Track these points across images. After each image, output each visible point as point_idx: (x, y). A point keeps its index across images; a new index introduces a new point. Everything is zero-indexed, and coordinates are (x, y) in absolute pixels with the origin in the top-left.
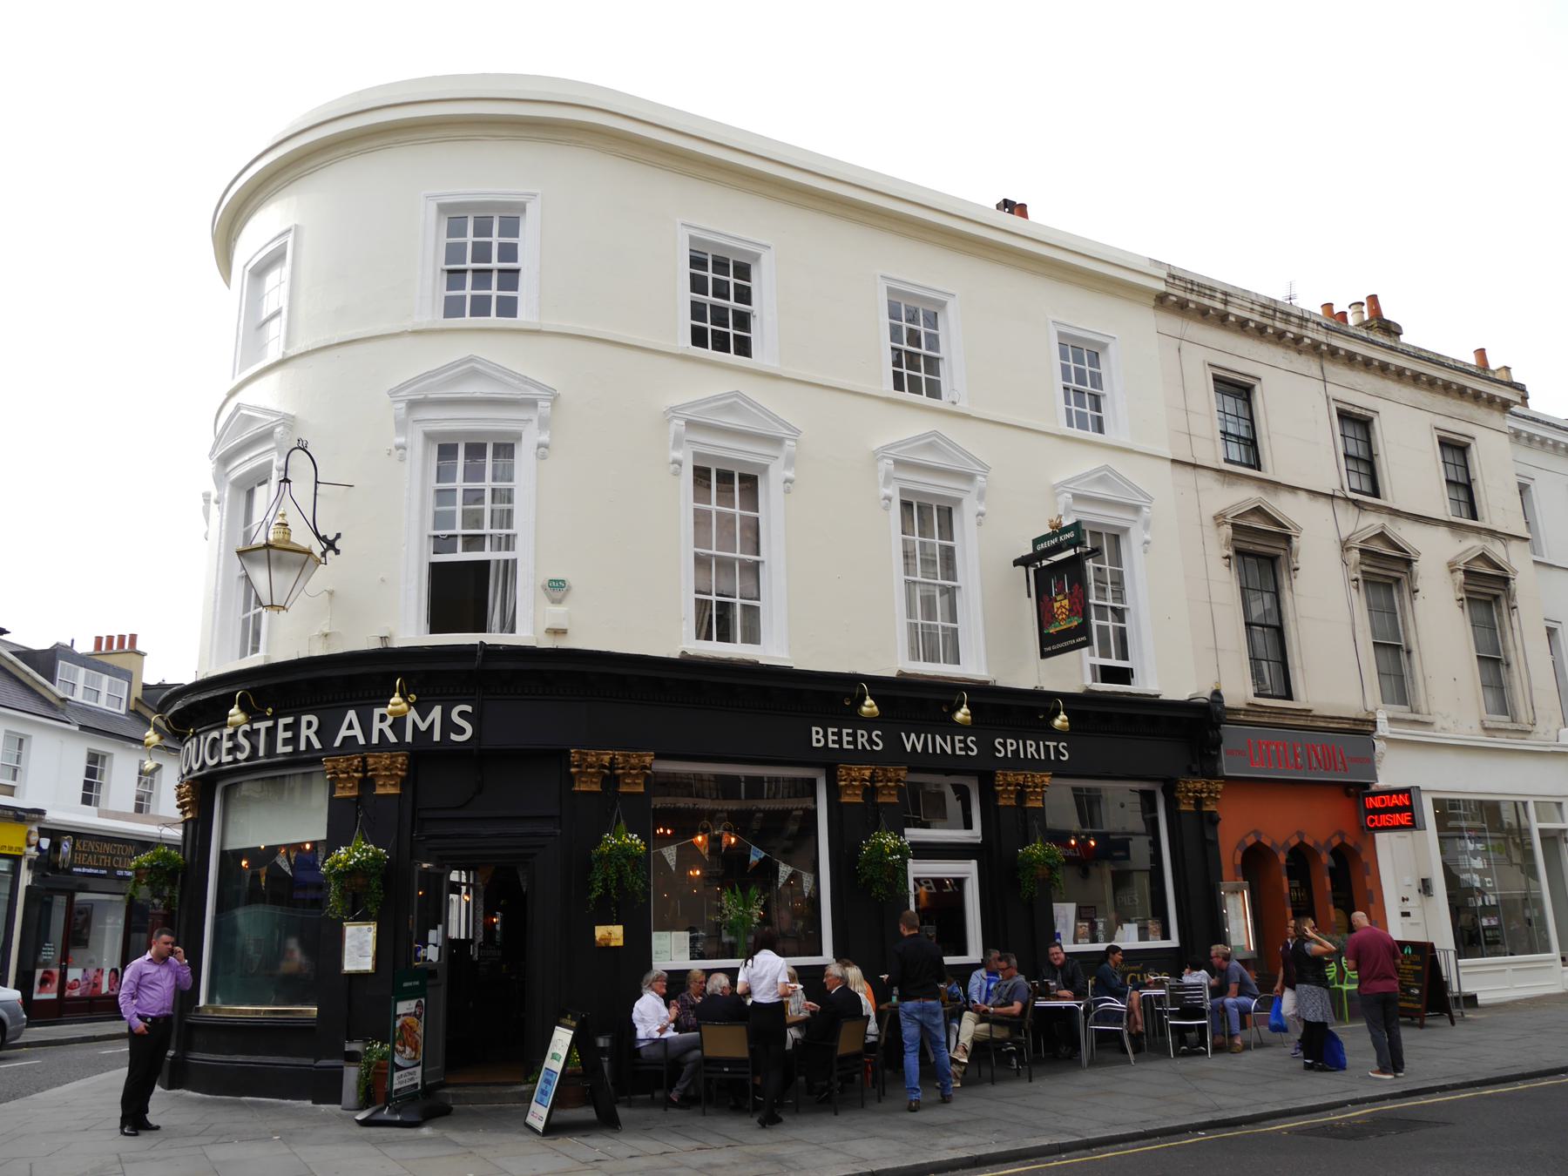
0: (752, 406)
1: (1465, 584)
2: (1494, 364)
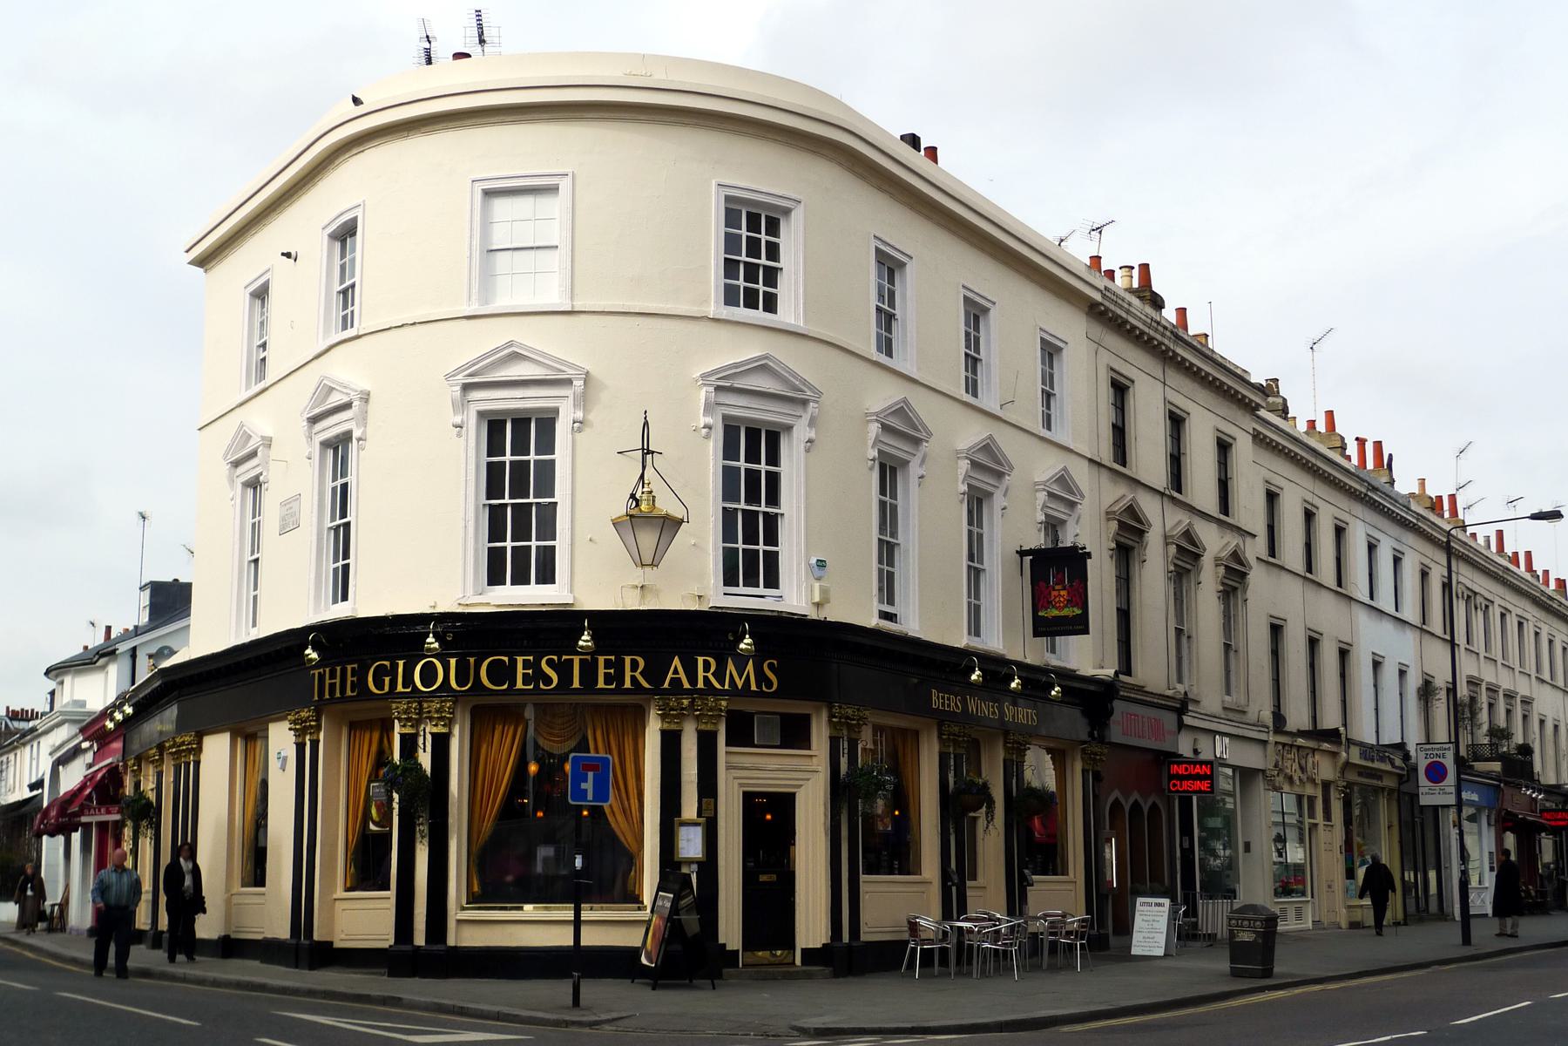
0: (910, 411)
2: (1193, 329)
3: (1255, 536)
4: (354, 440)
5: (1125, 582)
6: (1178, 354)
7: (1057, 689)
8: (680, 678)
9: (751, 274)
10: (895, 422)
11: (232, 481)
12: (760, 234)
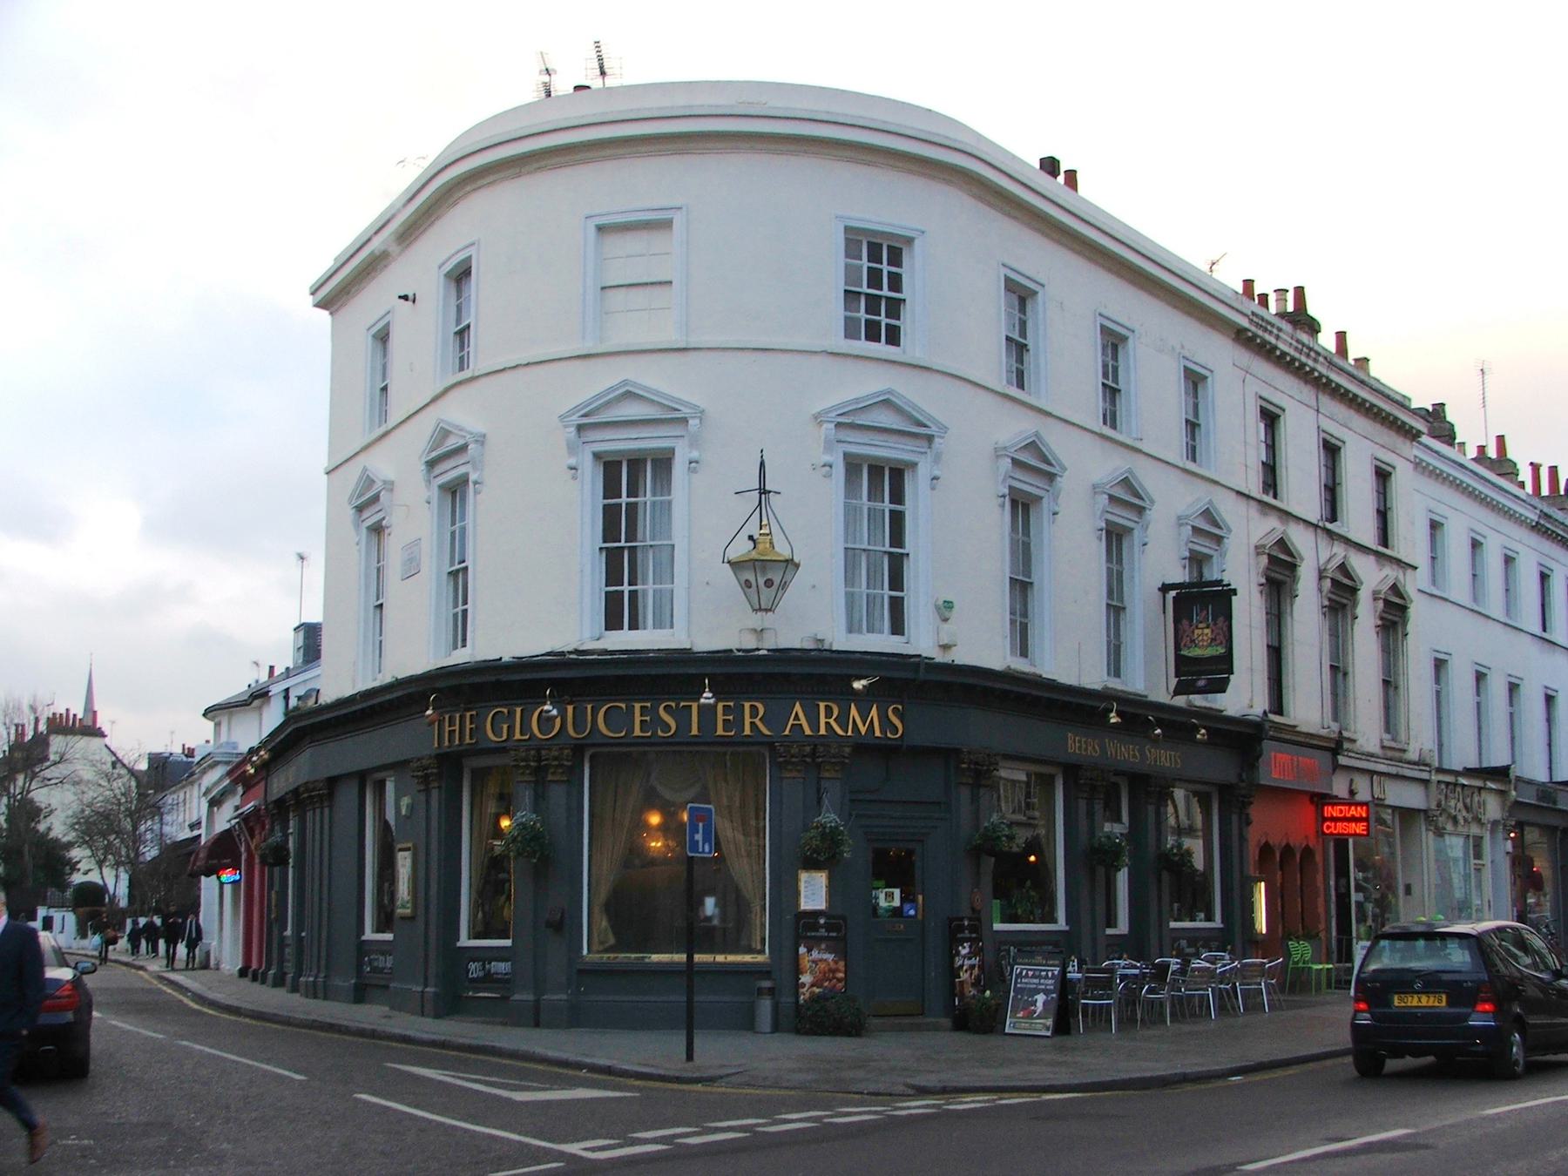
1: (1268, 569)
2: (1353, 354)
3: (1416, 568)
4: (471, 484)
5: (1276, 618)
6: (1332, 381)
7: (1203, 731)
8: (801, 725)
9: (873, 304)
10: (1024, 457)
11: (357, 527)
12: (882, 263)
